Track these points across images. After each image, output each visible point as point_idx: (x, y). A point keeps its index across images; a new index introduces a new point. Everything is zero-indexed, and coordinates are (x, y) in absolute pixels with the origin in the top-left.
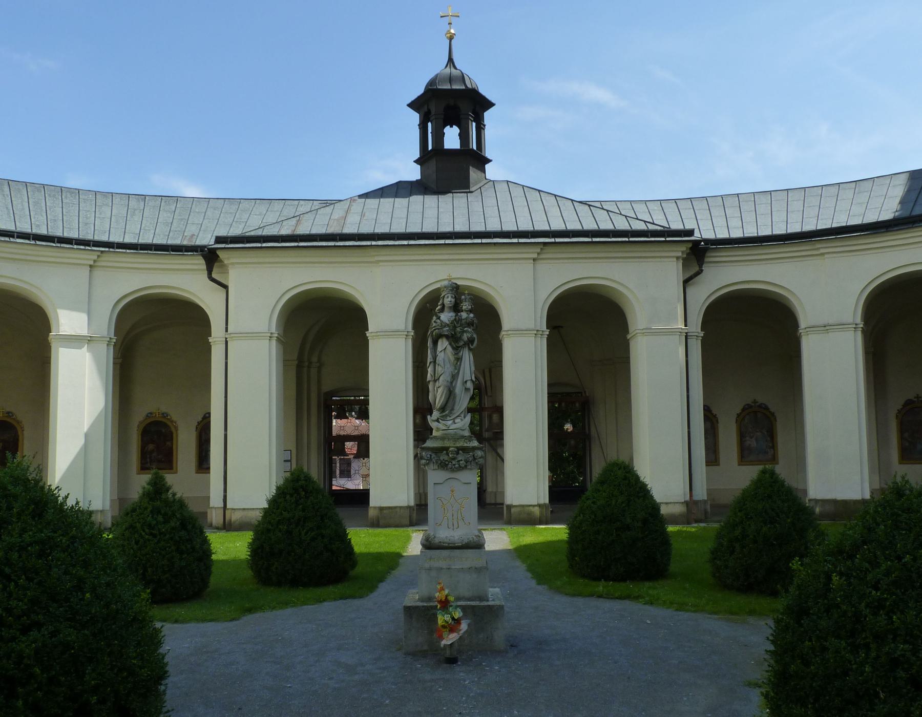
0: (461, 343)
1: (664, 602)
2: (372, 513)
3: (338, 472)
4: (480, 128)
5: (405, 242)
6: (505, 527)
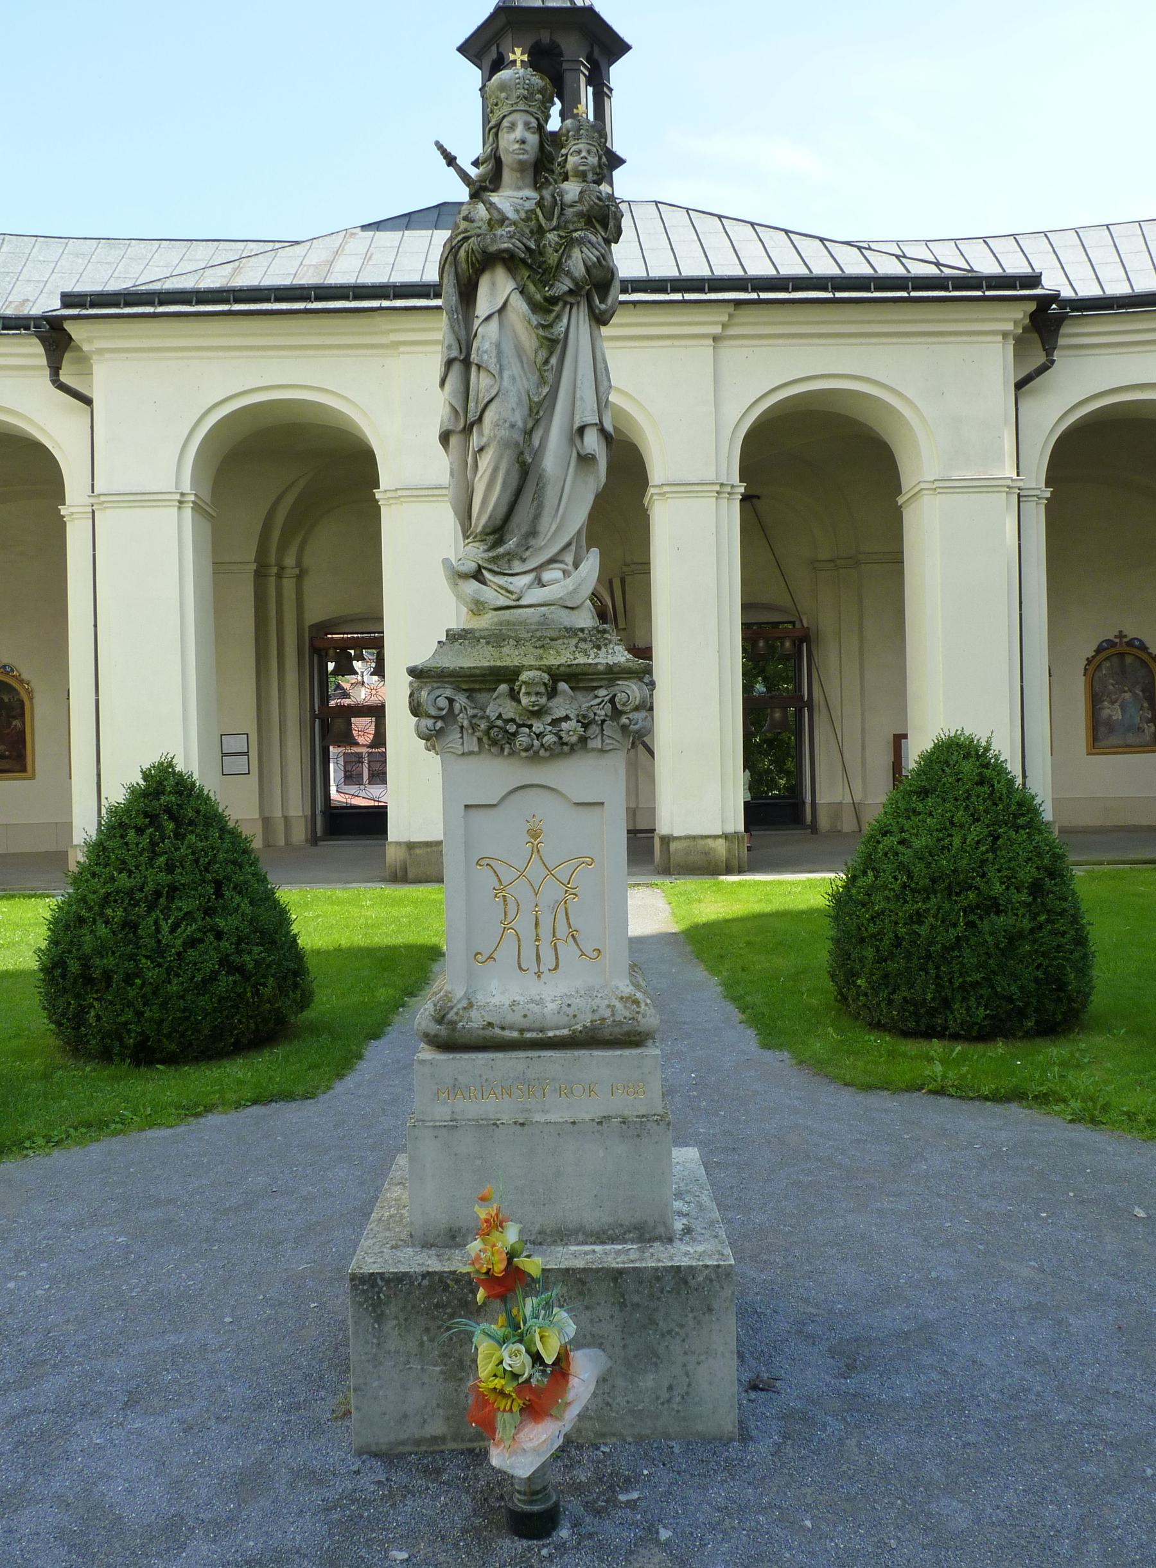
0: (563, 286)
1: (1131, 1116)
2: (393, 855)
4: (602, 94)
6: (658, 880)
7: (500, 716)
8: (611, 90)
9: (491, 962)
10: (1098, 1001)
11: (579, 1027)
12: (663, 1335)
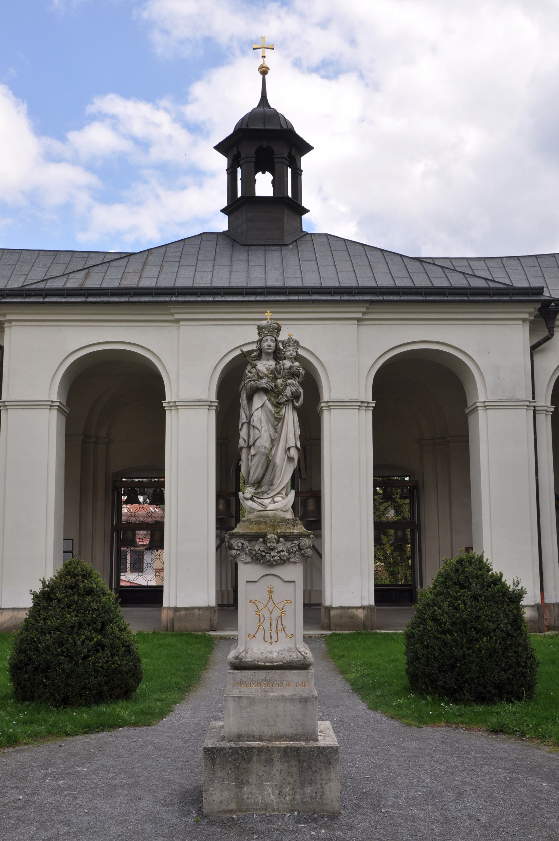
2: (164, 615)
3: (128, 565)
5: (210, 299)
7: (259, 550)
8: (302, 171)
9: (254, 638)
10: (539, 688)
11: (285, 662)
12: (314, 773)
